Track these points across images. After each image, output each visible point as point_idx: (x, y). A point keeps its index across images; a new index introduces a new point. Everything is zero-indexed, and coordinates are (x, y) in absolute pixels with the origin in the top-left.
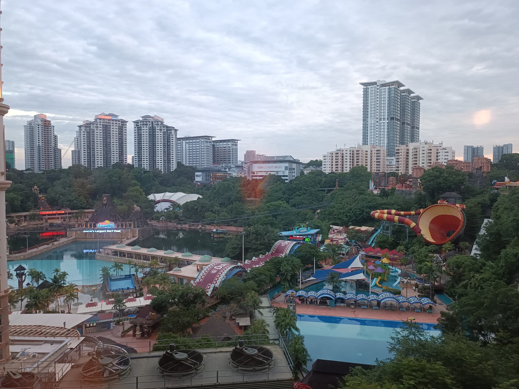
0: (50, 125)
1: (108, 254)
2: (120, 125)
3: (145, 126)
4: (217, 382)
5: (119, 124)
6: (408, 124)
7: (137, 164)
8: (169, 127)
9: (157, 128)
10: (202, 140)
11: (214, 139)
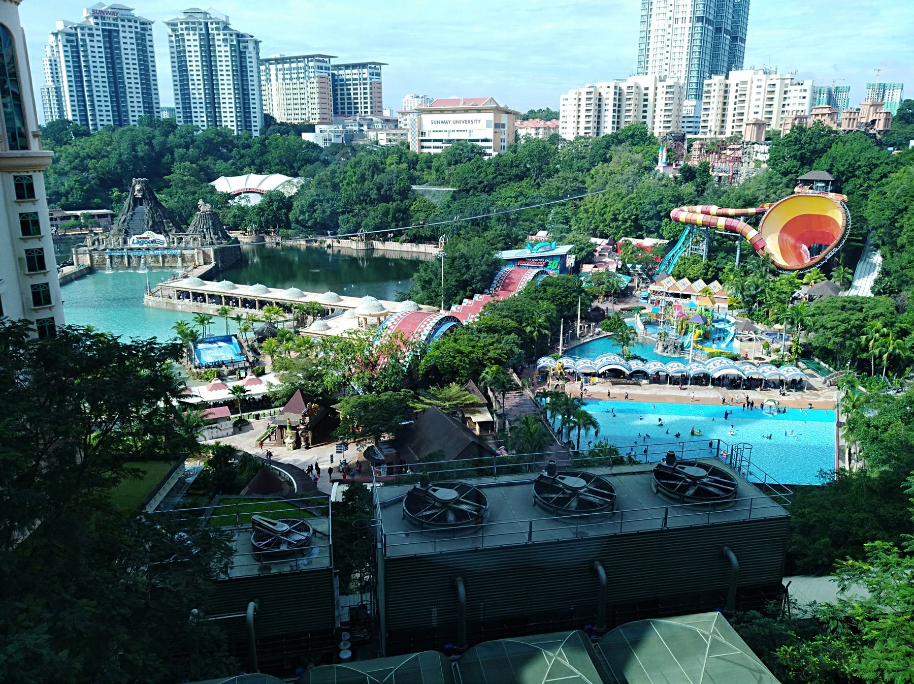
1: (170, 298)
2: (139, 30)
3: (191, 33)
4: (665, 526)
5: (136, 28)
6: (726, 32)
7: (181, 115)
8: (243, 36)
9: (217, 37)
10: (311, 64)
11: (334, 62)
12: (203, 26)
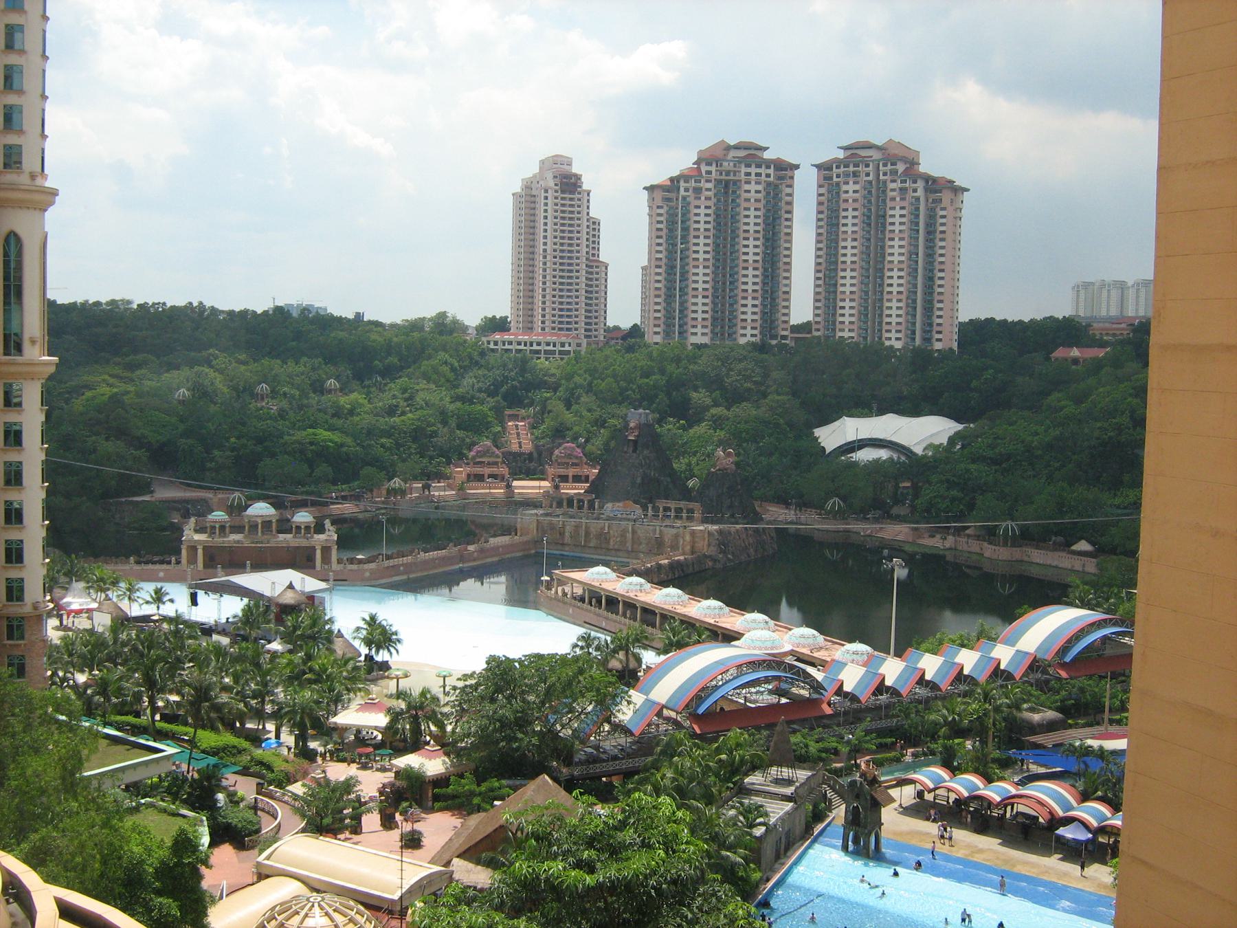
0: (580, 187)
5: (768, 176)
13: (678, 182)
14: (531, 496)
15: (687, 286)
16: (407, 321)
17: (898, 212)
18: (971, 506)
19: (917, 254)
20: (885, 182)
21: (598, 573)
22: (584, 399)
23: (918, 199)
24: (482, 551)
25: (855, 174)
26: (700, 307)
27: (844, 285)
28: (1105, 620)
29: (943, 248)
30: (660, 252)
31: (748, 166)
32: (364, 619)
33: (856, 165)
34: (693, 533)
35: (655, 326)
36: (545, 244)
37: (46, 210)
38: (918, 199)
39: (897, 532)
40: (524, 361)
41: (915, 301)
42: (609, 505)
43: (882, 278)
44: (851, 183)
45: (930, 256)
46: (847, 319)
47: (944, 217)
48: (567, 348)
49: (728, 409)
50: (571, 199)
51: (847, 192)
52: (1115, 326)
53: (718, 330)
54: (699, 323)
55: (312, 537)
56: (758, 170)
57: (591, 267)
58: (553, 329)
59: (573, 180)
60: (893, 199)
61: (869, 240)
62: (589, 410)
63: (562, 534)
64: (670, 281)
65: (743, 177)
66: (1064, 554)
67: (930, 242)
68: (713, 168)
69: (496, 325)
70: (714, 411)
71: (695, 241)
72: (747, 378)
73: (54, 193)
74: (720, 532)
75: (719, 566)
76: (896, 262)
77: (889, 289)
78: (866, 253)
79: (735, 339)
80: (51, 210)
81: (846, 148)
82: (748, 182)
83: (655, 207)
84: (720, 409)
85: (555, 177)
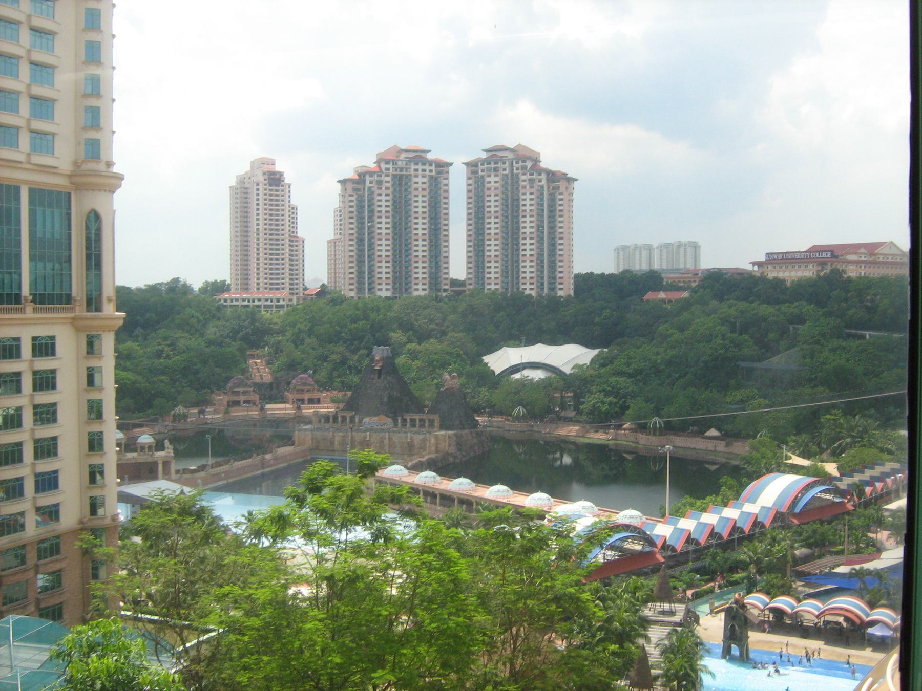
0: (283, 181)
2: (434, 173)
5: (431, 171)
12: (507, 165)
13: (364, 176)
14: (280, 416)
15: (373, 254)
16: (149, 286)
17: (528, 197)
18: (625, 408)
19: (543, 227)
20: (517, 175)
21: (395, 471)
22: (308, 341)
23: (542, 187)
24: (275, 459)
25: (496, 169)
26: (384, 270)
27: (490, 251)
28: (815, 481)
29: (561, 222)
30: (352, 229)
31: (417, 164)
32: (243, 516)
33: (496, 163)
34: (436, 437)
35: (350, 284)
36: (258, 225)
37: (114, 192)
38: (542, 187)
39: (571, 431)
40: (253, 314)
41: (542, 261)
42: (367, 420)
43: (518, 244)
44: (493, 176)
45: (552, 228)
46: (493, 276)
47: (561, 200)
48: (281, 303)
49: (420, 344)
50: (277, 191)
51: (490, 182)
52: (684, 275)
53: (397, 286)
54: (384, 281)
55: (153, 454)
56: (424, 167)
57: (292, 241)
58: (266, 288)
59: (277, 176)
60: (524, 187)
61: (507, 217)
62: (313, 349)
63: (332, 443)
64: (361, 251)
65: (412, 172)
66: (699, 439)
67: (552, 218)
68: (390, 166)
69: (219, 288)
70: (408, 346)
71: (379, 220)
72: (431, 321)
73: (120, 178)
74: (456, 435)
75: (458, 461)
76: (528, 233)
77: (524, 253)
78: (505, 227)
79: (410, 293)
80: (118, 192)
81: (487, 151)
82: (417, 176)
83: (347, 196)
84: (413, 345)
85: (264, 174)
